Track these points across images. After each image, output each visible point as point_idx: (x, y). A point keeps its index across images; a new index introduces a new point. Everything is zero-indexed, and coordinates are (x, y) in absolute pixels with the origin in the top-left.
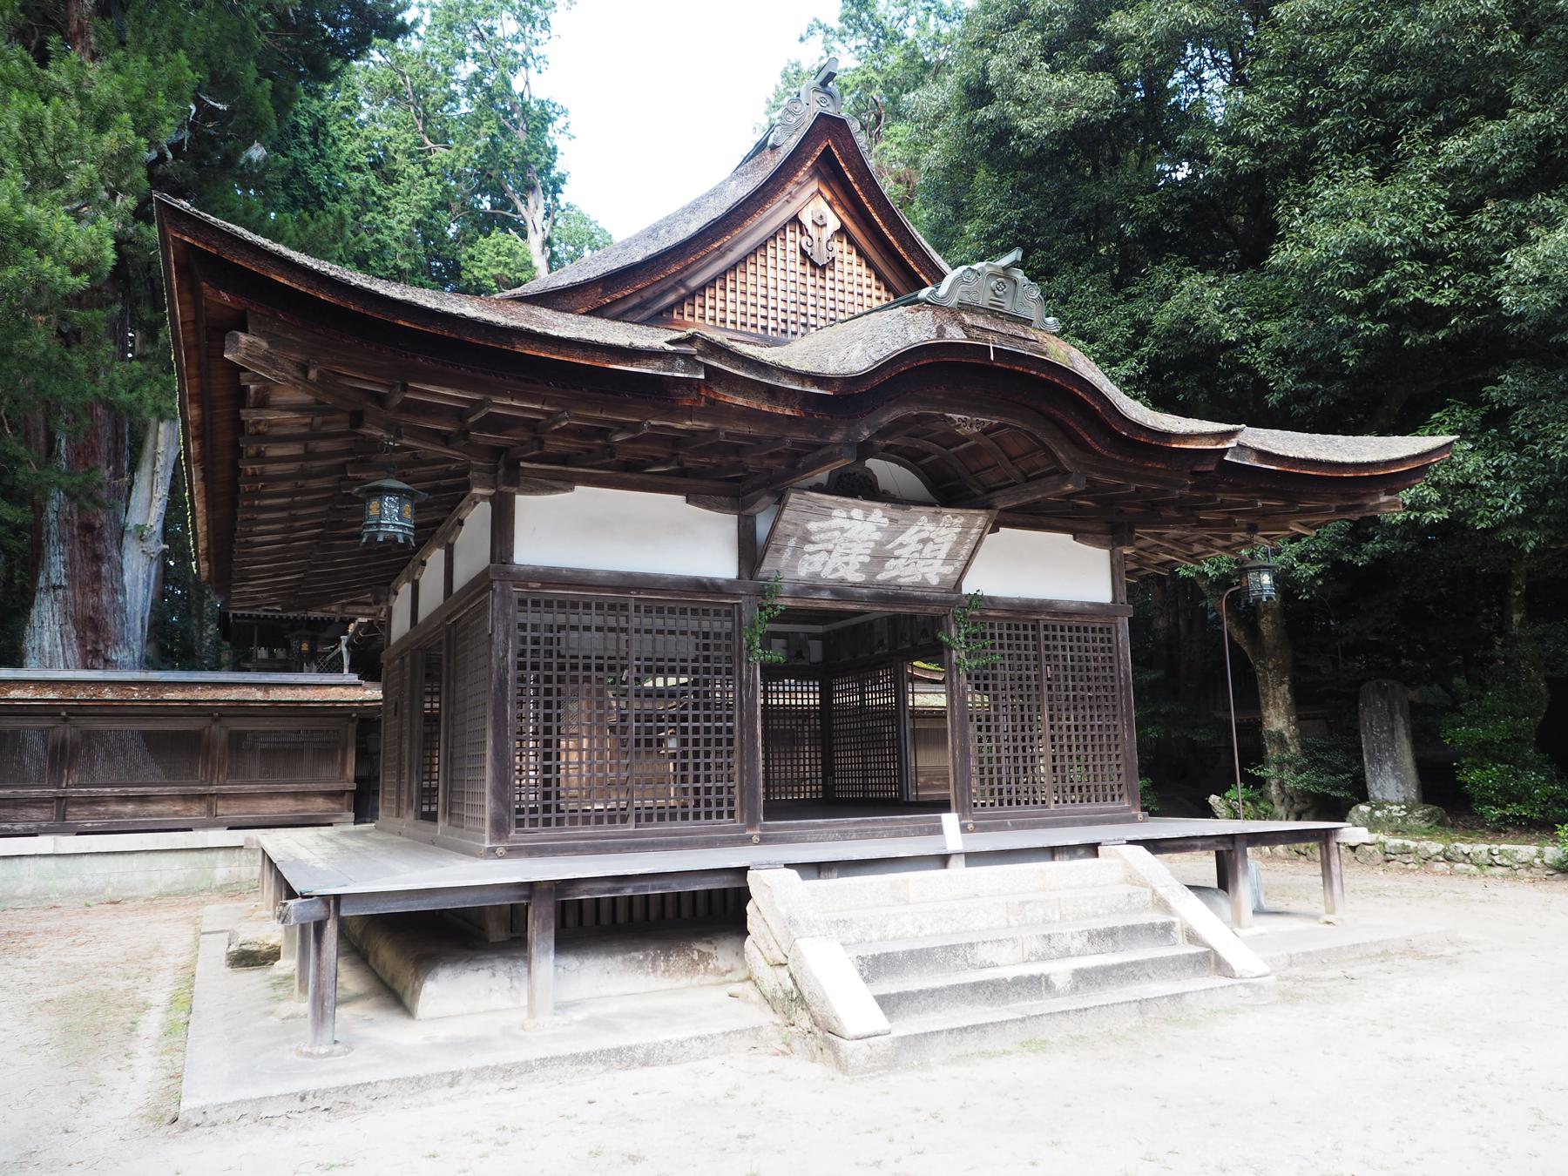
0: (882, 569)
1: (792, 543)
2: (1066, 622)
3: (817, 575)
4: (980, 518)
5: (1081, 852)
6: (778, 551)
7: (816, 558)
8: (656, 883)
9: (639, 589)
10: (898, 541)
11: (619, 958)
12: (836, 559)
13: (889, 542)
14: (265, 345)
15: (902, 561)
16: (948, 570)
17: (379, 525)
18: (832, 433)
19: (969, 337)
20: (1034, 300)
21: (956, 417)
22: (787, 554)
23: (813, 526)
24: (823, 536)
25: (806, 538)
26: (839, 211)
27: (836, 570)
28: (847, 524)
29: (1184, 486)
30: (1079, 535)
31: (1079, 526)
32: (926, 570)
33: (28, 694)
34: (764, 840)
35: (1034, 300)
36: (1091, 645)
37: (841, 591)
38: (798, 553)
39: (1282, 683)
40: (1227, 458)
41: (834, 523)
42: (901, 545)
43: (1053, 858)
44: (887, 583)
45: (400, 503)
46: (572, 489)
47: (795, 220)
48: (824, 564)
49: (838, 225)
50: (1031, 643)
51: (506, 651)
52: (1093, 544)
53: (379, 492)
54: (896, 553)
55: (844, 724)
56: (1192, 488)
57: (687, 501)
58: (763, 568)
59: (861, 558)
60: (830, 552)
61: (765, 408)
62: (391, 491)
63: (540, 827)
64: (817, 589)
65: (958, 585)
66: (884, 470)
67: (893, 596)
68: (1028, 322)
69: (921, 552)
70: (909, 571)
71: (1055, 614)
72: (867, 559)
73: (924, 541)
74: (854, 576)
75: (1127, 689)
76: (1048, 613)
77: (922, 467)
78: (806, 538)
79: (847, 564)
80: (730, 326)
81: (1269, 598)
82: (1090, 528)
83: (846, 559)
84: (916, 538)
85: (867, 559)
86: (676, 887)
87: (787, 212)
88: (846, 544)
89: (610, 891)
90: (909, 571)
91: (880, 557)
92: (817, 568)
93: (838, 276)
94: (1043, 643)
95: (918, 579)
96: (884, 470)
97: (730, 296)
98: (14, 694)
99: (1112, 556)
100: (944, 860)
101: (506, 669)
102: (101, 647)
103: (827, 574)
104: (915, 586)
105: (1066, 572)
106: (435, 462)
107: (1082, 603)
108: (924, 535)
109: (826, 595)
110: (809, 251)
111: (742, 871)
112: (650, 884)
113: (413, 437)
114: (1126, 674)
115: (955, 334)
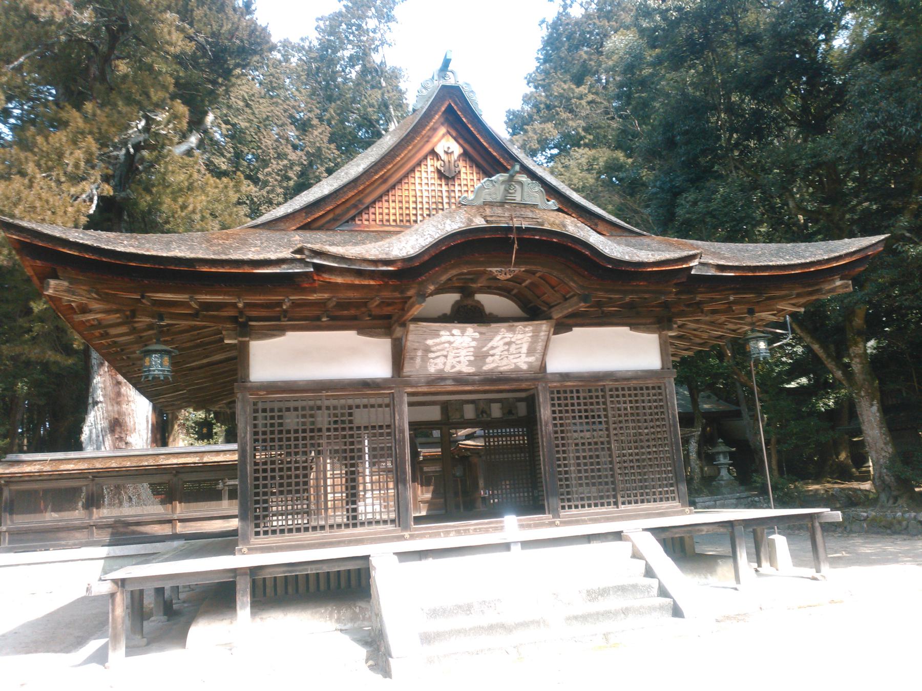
0: (485, 363)
1: (419, 353)
2: (625, 384)
3: (442, 370)
4: (544, 327)
5: (611, 537)
6: (412, 359)
7: (438, 361)
8: (313, 567)
9: (327, 390)
10: (490, 345)
11: (309, 612)
12: (451, 361)
13: (483, 347)
14: (66, 284)
15: (497, 357)
16: (531, 359)
17: (149, 371)
18: (408, 290)
19: (487, 221)
20: (536, 192)
21: (494, 270)
22: (418, 361)
23: (430, 342)
24: (438, 347)
25: (427, 350)
26: (461, 141)
27: (453, 367)
28: (451, 339)
29: (671, 292)
30: (634, 326)
31: (633, 321)
32: (515, 361)
33: (71, 466)
34: (412, 537)
35: (536, 192)
36: (646, 398)
37: (460, 379)
38: (425, 359)
39: (872, 405)
40: (693, 272)
41: (443, 339)
42: (493, 348)
43: (589, 542)
44: (491, 371)
45: (161, 357)
46: (284, 335)
47: (433, 153)
48: (445, 364)
49: (461, 151)
50: (601, 400)
51: (246, 433)
52: (644, 332)
53: (149, 353)
54: (491, 352)
55: (489, 458)
56: (676, 293)
57: (358, 334)
58: (405, 370)
59: (468, 358)
60: (446, 356)
61: (357, 282)
62: (156, 351)
63: (262, 536)
64: (443, 379)
65: (543, 367)
66: (490, 301)
67: (496, 380)
68: (535, 206)
69: (508, 350)
70: (505, 362)
71: (616, 380)
72: (472, 358)
73: (509, 344)
74: (467, 369)
75: (675, 426)
76: (611, 380)
77: (514, 295)
78: (427, 350)
79: (459, 362)
80: (392, 223)
81: (764, 358)
82: (644, 321)
83: (458, 359)
84: (501, 343)
85: (472, 358)
86: (325, 569)
87: (427, 148)
88: (453, 351)
89: (284, 572)
90: (505, 362)
91: (480, 356)
92: (440, 366)
93: (464, 182)
94: (609, 399)
95: (513, 367)
96: (490, 301)
97: (392, 205)
98: (63, 467)
99: (660, 338)
100: (506, 546)
101: (246, 443)
102: (123, 435)
103: (448, 369)
104: (512, 371)
105: (627, 351)
106: (187, 331)
107: (637, 371)
108: (507, 340)
109: (449, 382)
110: (442, 169)
111: (366, 558)
112: (309, 567)
113: (171, 319)
114: (674, 416)
115: (479, 222)
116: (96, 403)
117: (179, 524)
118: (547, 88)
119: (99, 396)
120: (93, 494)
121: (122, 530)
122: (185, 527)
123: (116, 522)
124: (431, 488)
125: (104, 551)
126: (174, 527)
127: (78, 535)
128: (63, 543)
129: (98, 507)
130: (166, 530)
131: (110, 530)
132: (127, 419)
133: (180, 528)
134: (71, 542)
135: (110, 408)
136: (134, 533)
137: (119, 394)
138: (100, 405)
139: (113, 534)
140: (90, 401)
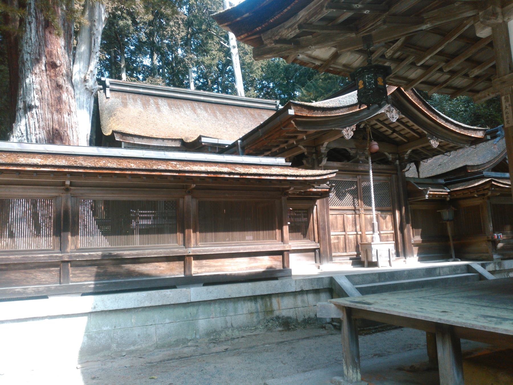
98: (22, 160)
116: (29, 108)
117: (194, 262)
118: (106, 109)
119: (34, 98)
120: (66, 212)
121: (111, 269)
122: (201, 267)
123: (104, 256)
124: (420, 230)
125: (91, 303)
126: (187, 267)
127: (42, 275)
128: (18, 289)
129: (75, 233)
130: (175, 270)
131: (94, 269)
132: (69, 132)
133: (197, 269)
134: (31, 288)
135: (48, 116)
136: (130, 274)
137: (59, 100)
138: (34, 111)
139: (98, 276)
140: (21, 105)
